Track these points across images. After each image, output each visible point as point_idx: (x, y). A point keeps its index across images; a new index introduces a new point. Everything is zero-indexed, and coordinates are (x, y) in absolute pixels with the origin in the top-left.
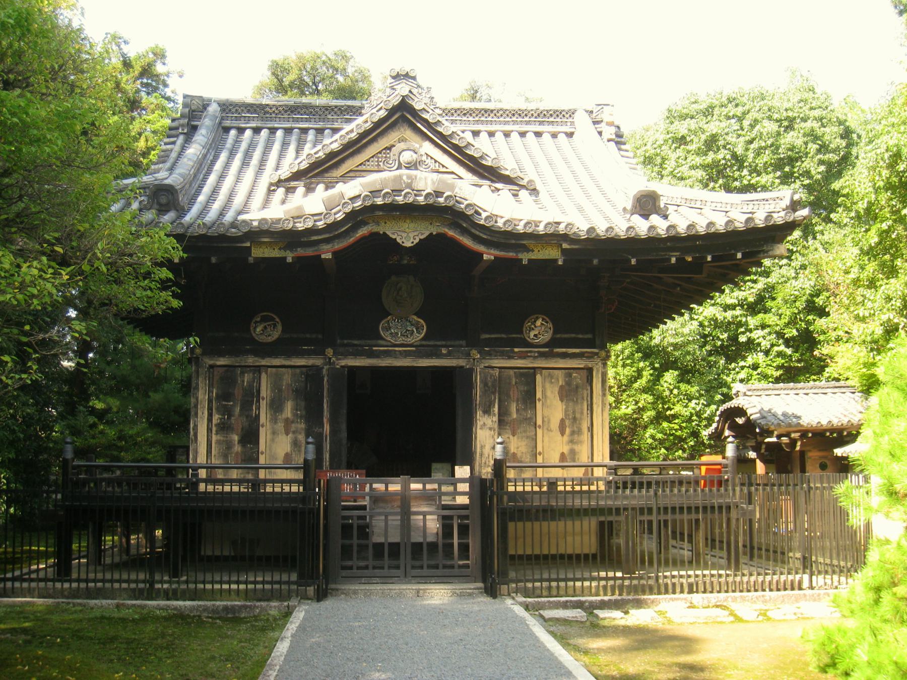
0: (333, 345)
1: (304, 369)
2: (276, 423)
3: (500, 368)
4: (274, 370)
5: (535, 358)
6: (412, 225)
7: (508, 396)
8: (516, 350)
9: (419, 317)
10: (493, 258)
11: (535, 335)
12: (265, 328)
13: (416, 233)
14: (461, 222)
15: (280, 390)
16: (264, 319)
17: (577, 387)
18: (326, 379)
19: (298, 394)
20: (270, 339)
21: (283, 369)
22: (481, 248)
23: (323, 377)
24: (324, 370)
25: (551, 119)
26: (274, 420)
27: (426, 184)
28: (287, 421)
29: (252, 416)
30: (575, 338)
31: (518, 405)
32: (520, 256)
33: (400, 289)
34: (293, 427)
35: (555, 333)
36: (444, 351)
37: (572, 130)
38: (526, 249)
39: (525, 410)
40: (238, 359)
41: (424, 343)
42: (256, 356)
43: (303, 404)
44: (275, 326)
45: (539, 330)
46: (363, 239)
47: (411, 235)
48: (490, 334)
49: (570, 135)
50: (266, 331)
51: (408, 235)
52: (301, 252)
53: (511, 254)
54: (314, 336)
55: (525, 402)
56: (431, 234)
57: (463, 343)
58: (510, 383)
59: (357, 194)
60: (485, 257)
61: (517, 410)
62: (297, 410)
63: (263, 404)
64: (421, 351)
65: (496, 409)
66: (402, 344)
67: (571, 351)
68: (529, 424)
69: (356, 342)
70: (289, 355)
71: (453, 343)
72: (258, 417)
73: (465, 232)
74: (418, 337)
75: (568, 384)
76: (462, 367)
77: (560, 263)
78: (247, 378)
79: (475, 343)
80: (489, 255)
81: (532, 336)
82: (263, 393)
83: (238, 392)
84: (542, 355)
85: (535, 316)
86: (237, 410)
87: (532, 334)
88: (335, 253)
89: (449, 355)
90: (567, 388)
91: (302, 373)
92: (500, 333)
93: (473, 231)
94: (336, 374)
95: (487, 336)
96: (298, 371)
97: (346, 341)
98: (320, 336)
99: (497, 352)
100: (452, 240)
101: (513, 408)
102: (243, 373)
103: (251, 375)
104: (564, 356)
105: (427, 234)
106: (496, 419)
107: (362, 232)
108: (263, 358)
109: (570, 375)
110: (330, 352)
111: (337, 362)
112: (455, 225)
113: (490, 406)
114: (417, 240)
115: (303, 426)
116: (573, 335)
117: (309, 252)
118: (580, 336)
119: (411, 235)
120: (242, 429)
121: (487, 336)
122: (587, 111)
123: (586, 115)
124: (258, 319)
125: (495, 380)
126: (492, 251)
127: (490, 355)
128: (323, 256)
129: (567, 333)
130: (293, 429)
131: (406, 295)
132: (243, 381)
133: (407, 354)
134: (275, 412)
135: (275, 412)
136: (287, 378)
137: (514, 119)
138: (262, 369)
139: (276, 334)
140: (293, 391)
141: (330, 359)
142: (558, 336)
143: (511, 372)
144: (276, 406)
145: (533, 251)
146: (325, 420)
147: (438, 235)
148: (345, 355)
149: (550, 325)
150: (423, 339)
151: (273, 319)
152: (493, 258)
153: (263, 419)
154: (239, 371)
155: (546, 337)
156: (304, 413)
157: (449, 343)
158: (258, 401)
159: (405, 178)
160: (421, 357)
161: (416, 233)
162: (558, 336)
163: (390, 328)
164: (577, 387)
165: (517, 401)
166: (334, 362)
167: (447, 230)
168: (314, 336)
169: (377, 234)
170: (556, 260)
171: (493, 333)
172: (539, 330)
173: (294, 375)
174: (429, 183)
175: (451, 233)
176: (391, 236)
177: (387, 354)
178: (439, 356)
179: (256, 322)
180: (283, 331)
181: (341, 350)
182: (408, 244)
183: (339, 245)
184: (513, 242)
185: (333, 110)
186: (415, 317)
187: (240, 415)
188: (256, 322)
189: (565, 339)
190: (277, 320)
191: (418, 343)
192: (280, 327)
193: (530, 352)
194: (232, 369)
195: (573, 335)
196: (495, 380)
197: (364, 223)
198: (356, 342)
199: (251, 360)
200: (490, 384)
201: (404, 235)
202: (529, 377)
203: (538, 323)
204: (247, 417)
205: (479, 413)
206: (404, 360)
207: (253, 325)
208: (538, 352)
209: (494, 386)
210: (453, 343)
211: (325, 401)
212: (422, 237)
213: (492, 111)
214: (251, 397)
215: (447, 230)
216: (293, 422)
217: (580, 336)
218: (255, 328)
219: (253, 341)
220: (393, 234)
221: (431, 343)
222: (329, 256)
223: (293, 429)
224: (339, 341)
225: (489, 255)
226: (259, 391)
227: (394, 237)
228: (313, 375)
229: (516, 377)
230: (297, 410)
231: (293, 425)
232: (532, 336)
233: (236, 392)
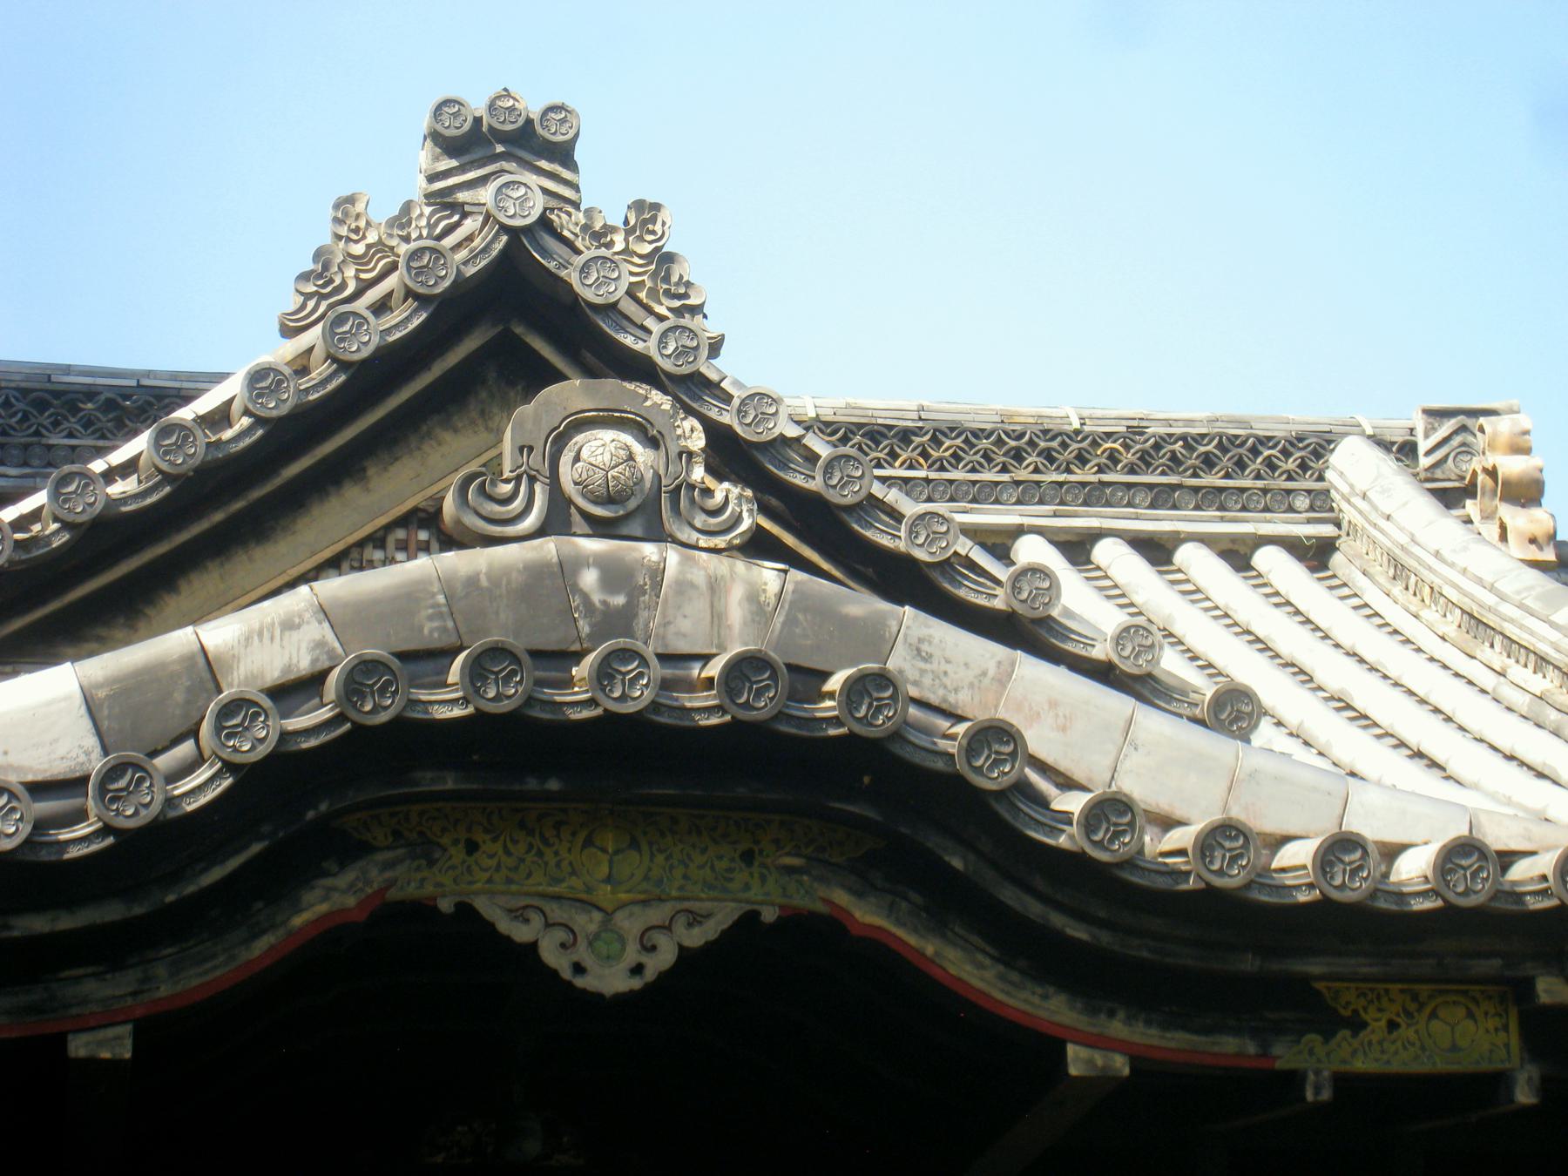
6: (633, 864)
10: (1120, 1064)
13: (656, 915)
14: (933, 841)
22: (1052, 1009)
25: (1212, 480)
27: (717, 617)
32: (1285, 1055)
37: (1327, 530)
38: (1328, 1020)
46: (333, 938)
47: (631, 924)
49: (1316, 555)
51: (612, 925)
53: (1232, 1047)
56: (751, 918)
59: (304, 664)
60: (1078, 1060)
73: (951, 903)
77: (1524, 1096)
80: (1098, 1049)
93: (1010, 896)
100: (880, 958)
105: (722, 917)
112: (898, 867)
114: (664, 958)
119: (631, 924)
122: (1384, 444)
123: (1386, 465)
126: (1117, 1028)
128: (79, 1047)
137: (1023, 474)
145: (1357, 1025)
147: (796, 925)
152: (1120, 1064)
159: (589, 579)
161: (656, 915)
167: (842, 898)
169: (421, 911)
170: (1497, 1082)
174: (736, 612)
175: (867, 915)
176: (505, 926)
182: (610, 980)
183: (177, 981)
184: (1249, 964)
185: (74, 410)
197: (336, 846)
201: (587, 923)
212: (696, 938)
213: (905, 436)
215: (842, 898)
220: (519, 914)
222: (112, 1044)
225: (1098, 1049)
227: (521, 933)
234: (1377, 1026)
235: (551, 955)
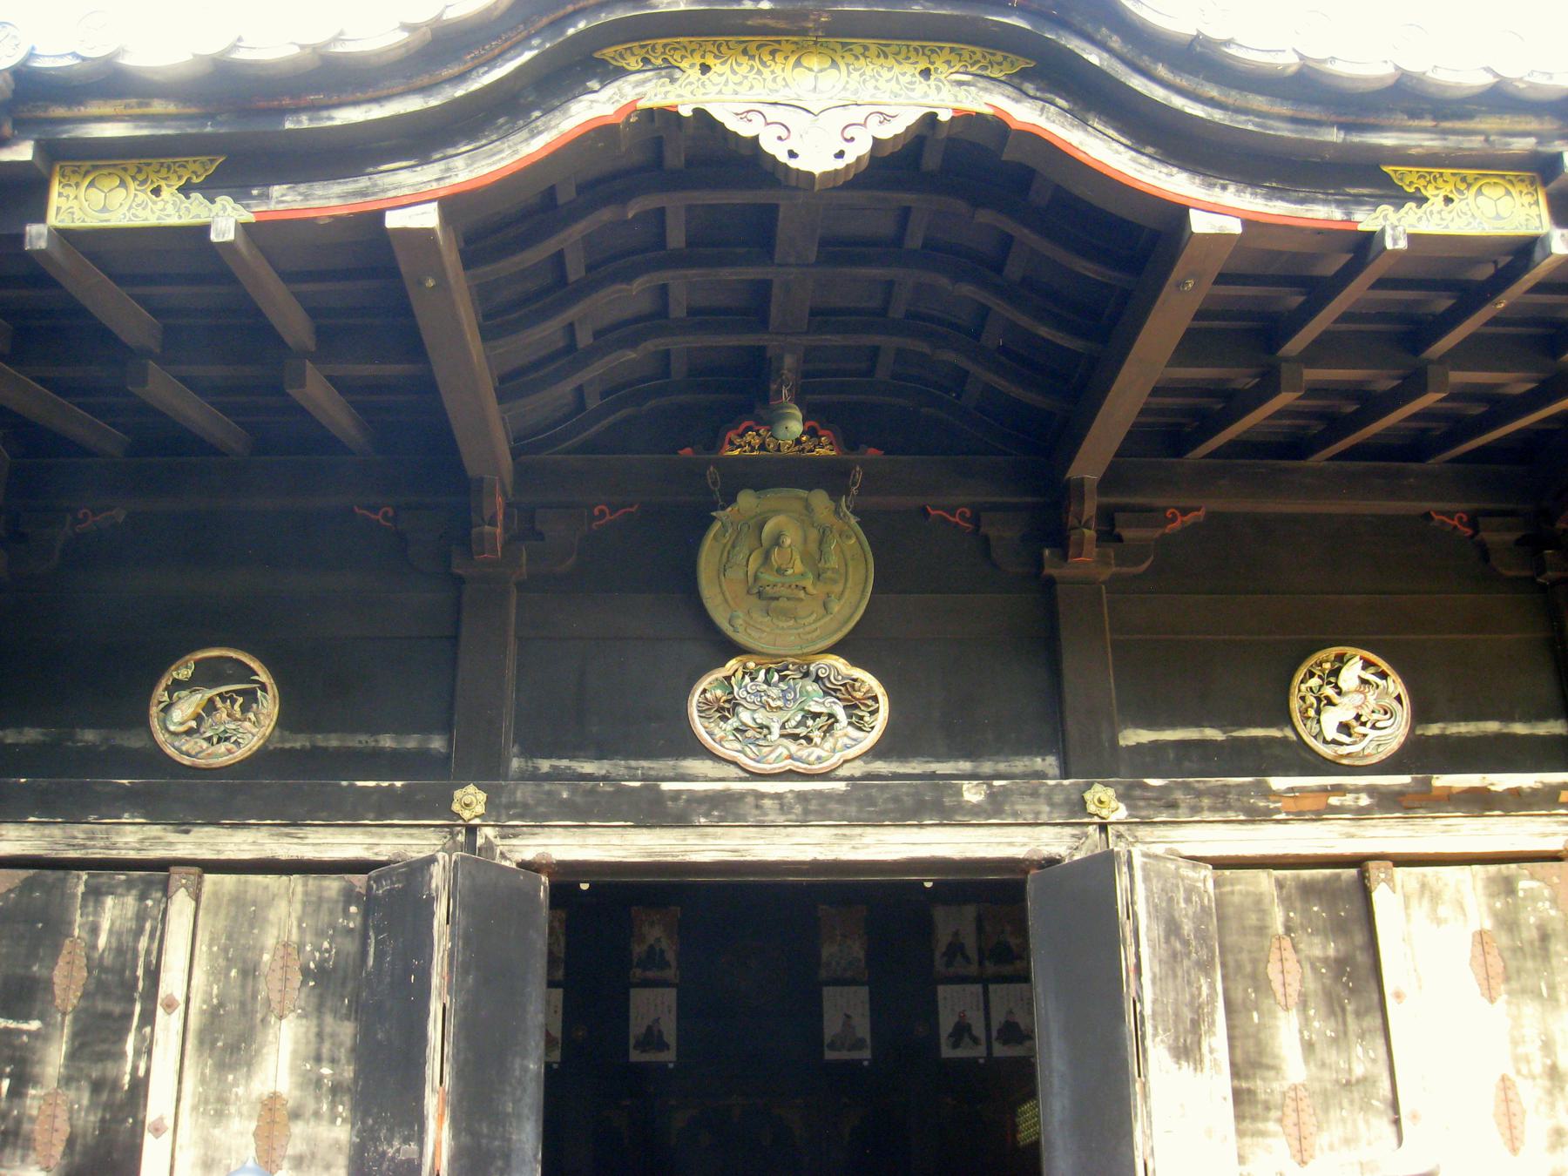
0: (488, 771)
1: (359, 880)
2: (220, 1115)
3: (1220, 864)
4: (229, 880)
5: (1361, 813)
7: (1260, 983)
8: (1278, 783)
9: (855, 661)
11: (1344, 728)
12: (210, 707)
15: (249, 972)
16: (208, 675)
17: (1545, 937)
18: (440, 911)
19: (325, 983)
20: (223, 755)
21: (269, 880)
23: (431, 901)
24: (437, 870)
26: (217, 1107)
28: (271, 1104)
29: (115, 1085)
30: (1499, 738)
31: (1306, 1022)
33: (777, 541)
34: (299, 1135)
35: (1420, 714)
36: (972, 793)
39: (1340, 1040)
40: (78, 831)
41: (881, 767)
42: (154, 818)
43: (346, 1031)
44: (250, 698)
45: (1358, 703)
48: (1151, 725)
50: (209, 720)
52: (284, 200)
53: (1323, 213)
54: (412, 742)
55: (1334, 1008)
57: (1049, 763)
58: (1261, 930)
60: (1200, 223)
61: (1309, 1047)
62: (318, 1059)
63: (167, 1027)
64: (866, 803)
65: (1216, 1042)
66: (789, 770)
67: (1501, 782)
68: (1366, 1107)
69: (588, 767)
70: (292, 817)
71: (1002, 767)
72: (140, 1087)
74: (848, 745)
75: (1508, 923)
76: (1052, 862)
78: (115, 912)
79: (1089, 758)
81: (1331, 732)
82: (172, 983)
83: (67, 980)
84: (1389, 802)
85: (1333, 652)
86: (55, 1057)
87: (1330, 720)
88: (451, 205)
89: (994, 810)
90: (1504, 939)
91: (349, 896)
92: (1198, 723)
94: (489, 895)
95: (1145, 736)
96: (333, 885)
97: (545, 765)
98: (437, 743)
99: (1199, 794)
101: (1286, 1033)
102: (95, 894)
103: (130, 901)
104: (1480, 802)
106: (1223, 1083)
107: (597, 105)
108: (184, 826)
109: (1508, 886)
110: (471, 800)
111: (501, 845)
113: (1196, 1024)
115: (342, 1133)
116: (1492, 727)
117: (327, 199)
118: (1519, 729)
120: (71, 1142)
121: (1145, 736)
124: (184, 673)
125: (1205, 910)
127: (1173, 805)
128: (393, 220)
129: (1467, 718)
130: (296, 1146)
131: (799, 566)
132: (94, 930)
133: (811, 810)
134: (222, 1067)
135: (222, 1067)
136: (285, 910)
138: (177, 876)
139: (253, 729)
140: (305, 972)
141: (472, 830)
142: (1434, 729)
143: (1264, 880)
144: (228, 1039)
145: (1421, 200)
146: (433, 1102)
147: (967, 120)
148: (540, 815)
149: (1395, 685)
150: (876, 752)
151: (246, 673)
152: (1234, 227)
153: (158, 1105)
154: (80, 882)
155: (1394, 733)
156: (348, 1073)
157: (987, 767)
158: (148, 1018)
160: (875, 822)
161: (857, 115)
162: (1434, 729)
163: (734, 705)
164: (1545, 937)
165: (1304, 1004)
166: (489, 846)
168: (412, 742)
169: (668, 116)
171: (1172, 725)
172: (1358, 703)
173: (313, 904)
175: (1025, 113)
176: (733, 124)
177: (724, 808)
178: (948, 813)
179: (178, 685)
180: (282, 723)
181: (524, 792)
183: (473, 167)
186: (840, 663)
187: (67, 1080)
188: (178, 685)
189: (1461, 740)
190: (264, 676)
191: (858, 769)
192: (269, 706)
193: (1339, 790)
194: (50, 875)
195: (1492, 727)
196: (1205, 910)
198: (588, 767)
199: (133, 838)
200: (1187, 928)
202: (1343, 896)
203: (1351, 674)
204: (97, 1087)
205: (1157, 1053)
206: (801, 834)
207: (161, 694)
208: (1371, 790)
209: (1202, 936)
210: (1002, 767)
211: (435, 1007)
214: (122, 994)
216: (296, 1115)
217: (1519, 729)
218: (167, 709)
219: (155, 762)
221: (915, 767)
222: (427, 217)
223: (296, 1146)
224: (515, 763)
225: (1218, 210)
226: (154, 975)
228: (392, 899)
229: (1287, 902)
230: (318, 1059)
231: (298, 1128)
232: (1331, 732)
233: (59, 976)
234: (1436, 202)
235: (769, 145)
